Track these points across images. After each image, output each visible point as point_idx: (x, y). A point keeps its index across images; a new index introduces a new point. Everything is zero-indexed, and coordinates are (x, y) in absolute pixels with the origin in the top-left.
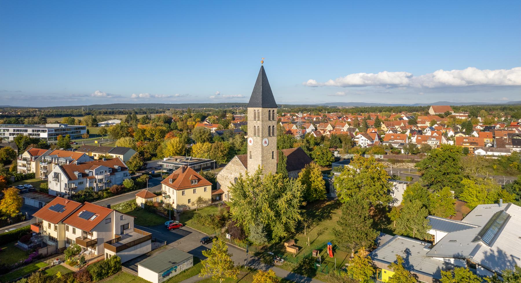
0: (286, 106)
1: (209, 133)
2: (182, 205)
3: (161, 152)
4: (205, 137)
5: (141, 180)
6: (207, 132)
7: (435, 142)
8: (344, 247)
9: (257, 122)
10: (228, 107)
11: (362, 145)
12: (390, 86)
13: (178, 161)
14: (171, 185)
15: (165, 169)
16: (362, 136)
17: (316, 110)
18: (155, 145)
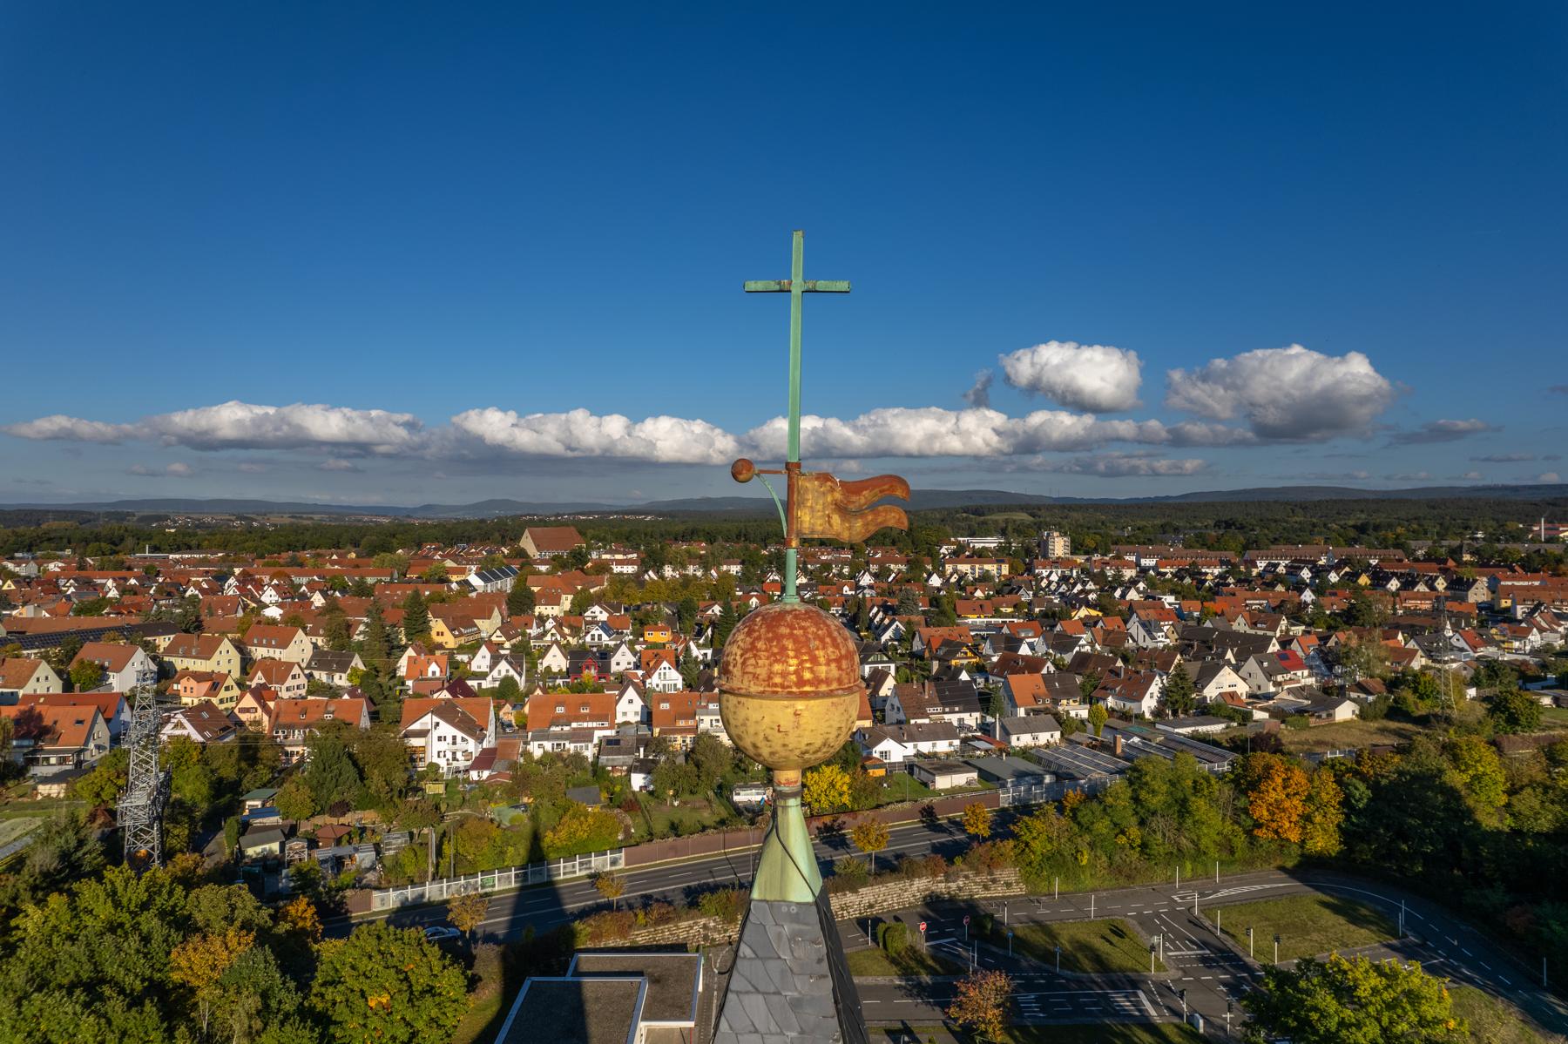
8: (431, 970)
11: (442, 762)
16: (442, 723)
17: (97, 538)
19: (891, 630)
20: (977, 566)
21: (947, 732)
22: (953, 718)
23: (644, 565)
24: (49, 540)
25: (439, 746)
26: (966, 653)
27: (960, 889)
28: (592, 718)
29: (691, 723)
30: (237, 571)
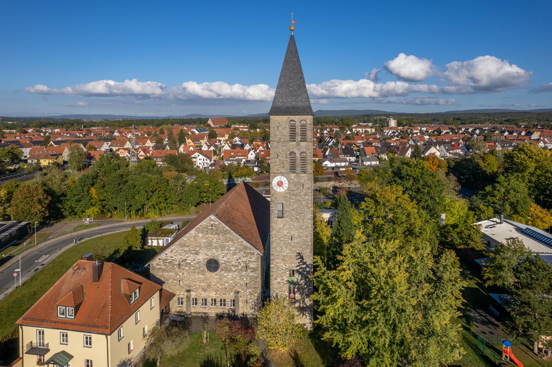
9: (298, 145)
14: (74, 324)
16: (200, 155)
20: (364, 129)
21: (345, 161)
22: (348, 158)
23: (250, 128)
24: (50, 124)
25: (199, 162)
27: (342, 185)
28: (242, 156)
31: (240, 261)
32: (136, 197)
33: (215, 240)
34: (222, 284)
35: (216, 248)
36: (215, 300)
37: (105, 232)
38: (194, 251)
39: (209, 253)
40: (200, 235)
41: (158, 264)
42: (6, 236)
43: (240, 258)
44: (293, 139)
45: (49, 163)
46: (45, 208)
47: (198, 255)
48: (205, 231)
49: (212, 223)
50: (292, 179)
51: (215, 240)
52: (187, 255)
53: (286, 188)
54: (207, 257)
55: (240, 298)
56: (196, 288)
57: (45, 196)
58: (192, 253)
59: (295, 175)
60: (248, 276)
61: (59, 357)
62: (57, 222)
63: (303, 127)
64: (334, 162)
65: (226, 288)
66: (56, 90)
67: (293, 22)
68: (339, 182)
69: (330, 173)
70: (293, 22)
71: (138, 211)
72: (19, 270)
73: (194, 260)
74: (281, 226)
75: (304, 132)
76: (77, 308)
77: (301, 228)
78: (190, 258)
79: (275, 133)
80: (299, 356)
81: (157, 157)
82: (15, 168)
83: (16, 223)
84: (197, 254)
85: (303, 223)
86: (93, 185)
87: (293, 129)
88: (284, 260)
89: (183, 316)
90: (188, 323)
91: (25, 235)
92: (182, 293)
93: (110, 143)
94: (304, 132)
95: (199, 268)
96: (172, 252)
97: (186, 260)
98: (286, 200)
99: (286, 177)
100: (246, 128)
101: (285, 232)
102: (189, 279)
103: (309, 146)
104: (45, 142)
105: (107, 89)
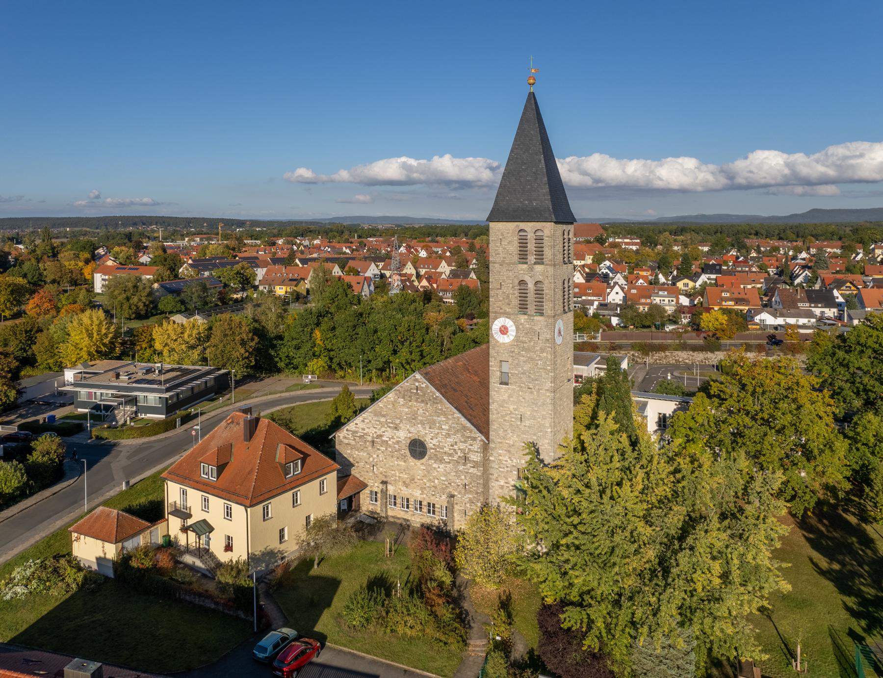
0: (255, 223)
1: (148, 290)
2: (264, 554)
3: (52, 349)
4: (140, 300)
5: (45, 459)
6: (144, 288)
7: (667, 299)
9: (531, 269)
10: (125, 225)
12: (457, 185)
13: (123, 378)
15: (83, 405)
18: (26, 332)
19: (801, 276)
21: (810, 315)
24: (310, 231)
26: (850, 287)
29: (648, 301)
30: (404, 245)
31: (456, 447)
32: (376, 349)
33: (421, 411)
34: (430, 480)
35: (423, 424)
36: (421, 503)
37: (325, 398)
38: (392, 423)
39: (412, 429)
40: (401, 401)
41: (345, 437)
42: (199, 385)
43: (456, 442)
44: (524, 261)
45: (286, 292)
46: (249, 353)
47: (398, 430)
48: (407, 395)
49: (417, 384)
50: (521, 324)
51: (421, 411)
52: (383, 429)
53: (512, 338)
54: (409, 435)
55: (455, 506)
56: (395, 480)
57: (250, 335)
58: (389, 427)
59: (526, 317)
60: (467, 473)
61: (203, 530)
62: (269, 377)
63: (539, 240)
64: (782, 315)
65: (435, 487)
66: (324, 177)
67: (533, 71)
68: (767, 355)
69: (757, 337)
70: (533, 71)
71: (382, 370)
72: (198, 427)
73: (393, 438)
74: (506, 397)
75: (540, 249)
76: (221, 468)
77: (536, 404)
78: (388, 434)
79: (496, 250)
80: (512, 600)
81: (445, 291)
82: (242, 298)
83: (213, 369)
84: (396, 428)
85: (538, 396)
86: (318, 324)
87: (523, 244)
88: (509, 451)
89: (376, 519)
90: (379, 529)
91: (225, 389)
92: (376, 484)
93: (381, 264)
94: (540, 249)
95: (399, 450)
96: (363, 421)
97: (381, 436)
98: (513, 357)
99: (512, 320)
100: (636, 244)
101: (511, 407)
102: (385, 465)
103: (547, 271)
104: (288, 261)
105: (405, 172)
